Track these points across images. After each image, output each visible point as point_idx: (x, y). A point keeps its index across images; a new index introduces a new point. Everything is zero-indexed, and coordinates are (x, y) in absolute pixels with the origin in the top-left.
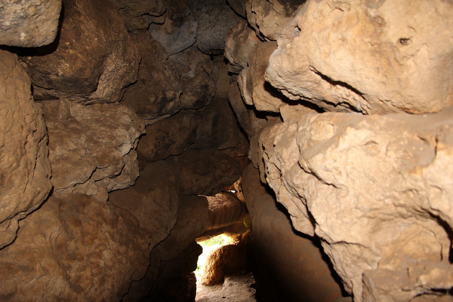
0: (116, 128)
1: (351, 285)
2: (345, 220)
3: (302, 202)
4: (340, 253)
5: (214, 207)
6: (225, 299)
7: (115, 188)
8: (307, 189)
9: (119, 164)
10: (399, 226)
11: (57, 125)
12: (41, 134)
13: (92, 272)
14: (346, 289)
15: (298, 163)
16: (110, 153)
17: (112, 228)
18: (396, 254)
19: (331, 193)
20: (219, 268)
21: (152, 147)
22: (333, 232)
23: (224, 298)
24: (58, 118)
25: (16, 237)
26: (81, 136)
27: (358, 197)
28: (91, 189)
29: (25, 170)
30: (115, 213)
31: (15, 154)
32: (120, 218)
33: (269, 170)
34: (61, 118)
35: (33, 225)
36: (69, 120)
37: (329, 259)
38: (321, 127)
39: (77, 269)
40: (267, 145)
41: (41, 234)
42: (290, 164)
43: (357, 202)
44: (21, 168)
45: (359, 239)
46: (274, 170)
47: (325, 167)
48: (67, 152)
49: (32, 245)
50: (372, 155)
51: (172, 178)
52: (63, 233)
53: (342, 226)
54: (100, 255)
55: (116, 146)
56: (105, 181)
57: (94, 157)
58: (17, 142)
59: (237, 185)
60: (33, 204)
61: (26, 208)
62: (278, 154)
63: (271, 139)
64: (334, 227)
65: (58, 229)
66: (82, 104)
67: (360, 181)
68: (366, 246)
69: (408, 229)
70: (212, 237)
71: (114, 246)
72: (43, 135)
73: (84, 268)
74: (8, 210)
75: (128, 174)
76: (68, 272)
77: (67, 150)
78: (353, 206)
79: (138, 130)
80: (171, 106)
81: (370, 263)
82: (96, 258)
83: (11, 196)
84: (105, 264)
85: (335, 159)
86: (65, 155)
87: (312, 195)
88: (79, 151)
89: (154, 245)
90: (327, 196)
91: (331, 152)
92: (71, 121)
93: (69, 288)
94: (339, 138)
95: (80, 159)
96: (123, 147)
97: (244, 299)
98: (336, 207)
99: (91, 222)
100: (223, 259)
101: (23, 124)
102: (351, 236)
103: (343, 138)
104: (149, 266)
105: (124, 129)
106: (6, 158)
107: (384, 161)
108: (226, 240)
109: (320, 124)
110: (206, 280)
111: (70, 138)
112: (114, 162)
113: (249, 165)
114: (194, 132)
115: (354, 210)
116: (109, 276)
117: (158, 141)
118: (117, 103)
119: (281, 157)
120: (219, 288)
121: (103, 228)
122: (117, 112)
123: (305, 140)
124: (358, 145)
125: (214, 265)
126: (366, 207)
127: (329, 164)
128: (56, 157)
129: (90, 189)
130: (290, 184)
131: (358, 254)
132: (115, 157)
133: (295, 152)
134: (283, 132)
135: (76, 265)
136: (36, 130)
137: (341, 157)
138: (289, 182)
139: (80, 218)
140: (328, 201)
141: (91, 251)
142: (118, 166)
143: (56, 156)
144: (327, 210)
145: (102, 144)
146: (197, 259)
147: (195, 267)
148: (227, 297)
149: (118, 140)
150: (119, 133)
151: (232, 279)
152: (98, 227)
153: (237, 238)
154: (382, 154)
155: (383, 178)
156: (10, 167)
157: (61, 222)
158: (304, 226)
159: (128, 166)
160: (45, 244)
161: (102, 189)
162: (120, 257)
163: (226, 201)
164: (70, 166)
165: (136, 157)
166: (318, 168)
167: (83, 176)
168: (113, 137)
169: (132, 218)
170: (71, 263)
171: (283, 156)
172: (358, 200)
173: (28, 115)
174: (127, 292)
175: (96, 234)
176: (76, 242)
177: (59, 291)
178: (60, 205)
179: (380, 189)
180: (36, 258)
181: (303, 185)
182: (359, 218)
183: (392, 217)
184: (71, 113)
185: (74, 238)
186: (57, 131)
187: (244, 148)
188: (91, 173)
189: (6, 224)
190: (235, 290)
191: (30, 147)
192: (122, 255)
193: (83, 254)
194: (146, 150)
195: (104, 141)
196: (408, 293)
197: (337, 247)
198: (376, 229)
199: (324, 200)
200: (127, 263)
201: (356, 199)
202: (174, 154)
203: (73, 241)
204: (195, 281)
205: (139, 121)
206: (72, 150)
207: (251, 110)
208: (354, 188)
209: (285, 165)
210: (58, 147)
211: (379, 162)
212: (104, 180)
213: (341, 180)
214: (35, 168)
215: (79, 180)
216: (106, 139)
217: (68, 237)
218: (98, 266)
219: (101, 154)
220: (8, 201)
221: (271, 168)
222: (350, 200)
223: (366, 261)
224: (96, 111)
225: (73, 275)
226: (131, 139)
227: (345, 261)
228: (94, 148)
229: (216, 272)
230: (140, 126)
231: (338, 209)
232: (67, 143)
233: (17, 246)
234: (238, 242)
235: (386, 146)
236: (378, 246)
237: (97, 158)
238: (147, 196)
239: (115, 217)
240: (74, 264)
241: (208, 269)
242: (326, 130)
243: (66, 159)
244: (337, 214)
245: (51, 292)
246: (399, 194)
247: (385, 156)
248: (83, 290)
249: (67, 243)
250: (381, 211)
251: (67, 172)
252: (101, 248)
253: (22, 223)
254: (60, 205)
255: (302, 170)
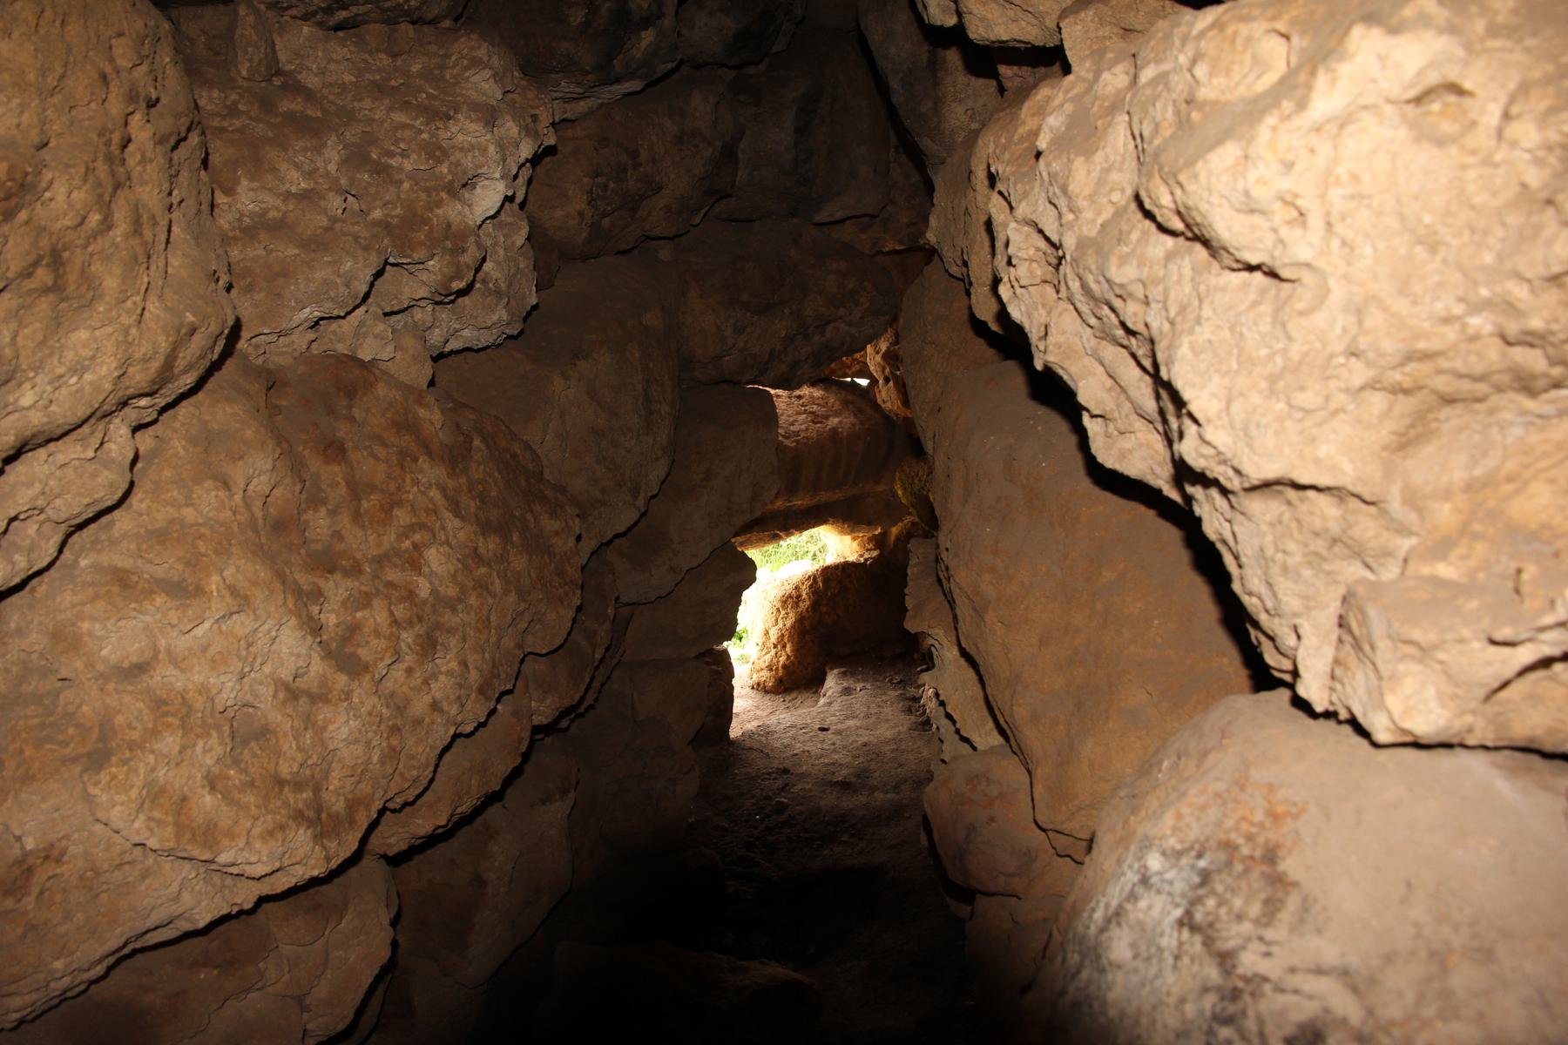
0: (449, 118)
1: (1291, 641)
2: (1301, 398)
3: (1134, 356)
4: (1264, 528)
5: (797, 434)
6: (828, 735)
7: (454, 345)
8: (1160, 298)
9: (464, 250)
10: (1502, 427)
11: (236, 103)
12: (177, 116)
13: (391, 613)
14: (1271, 658)
15: (1138, 199)
16: (431, 210)
17: (453, 474)
18: (1476, 527)
19: (1255, 304)
20: (808, 638)
21: (578, 203)
22: (1250, 445)
23: (822, 729)
24: (233, 73)
25: (132, 484)
26: (324, 145)
27: (1359, 312)
28: (374, 342)
29: (135, 241)
30: (458, 426)
31: (91, 178)
32: (477, 442)
33: (1011, 250)
34: (244, 73)
35: (184, 447)
36: (277, 82)
37: (1218, 556)
38: (1239, 48)
39: (344, 603)
40: (1009, 163)
41: (215, 478)
42: (1099, 213)
43: (1354, 331)
44: (118, 234)
45: (1346, 473)
46: (1032, 252)
47: (1247, 193)
48: (278, 202)
49: (188, 513)
50: (1441, 142)
51: (652, 319)
52: (288, 480)
53: (1288, 424)
54: (414, 562)
55: (451, 183)
56: (418, 315)
57: (375, 223)
58: (94, 136)
59: (878, 358)
60: (176, 371)
61: (153, 382)
62: (1053, 177)
63: (1021, 140)
64: (1258, 425)
65: (269, 466)
66: (320, 24)
67: (1375, 249)
68: (1368, 498)
69: (1533, 438)
70: (789, 534)
71: (462, 535)
72: (185, 121)
73: (365, 601)
74: (92, 383)
75: (498, 293)
76: (315, 609)
77: (278, 195)
78: (1340, 347)
79: (529, 130)
80: (644, 44)
81: (1370, 560)
82: (403, 570)
83: (97, 333)
84: (434, 592)
85: (1291, 157)
86: (273, 214)
87: (1179, 319)
88: (323, 198)
89: (594, 544)
90: (1239, 315)
91: (1274, 129)
92: (284, 86)
93: (322, 658)
94: (1313, 73)
95: (327, 229)
96: (478, 190)
97: (889, 734)
98: (1272, 356)
99: (382, 452)
100: (824, 609)
101: (108, 68)
102: (1317, 461)
103: (1329, 70)
104: (579, 609)
105: (478, 120)
106: (60, 191)
107: (1488, 162)
108: (833, 545)
109: (1236, 33)
110: (765, 674)
111: (286, 150)
112: (448, 244)
113: (927, 270)
114: (729, 154)
115: (1341, 360)
116: (451, 631)
117: (600, 180)
118: (447, 23)
119: (1064, 190)
120: (809, 702)
121: (421, 471)
122: (448, 56)
123: (1165, 108)
124: (1390, 101)
125: (793, 626)
126: (1388, 346)
127: (1264, 180)
128: (240, 220)
129: (370, 340)
130: (1094, 286)
131: (1335, 528)
132: (449, 225)
133: (1120, 170)
134: (1072, 100)
135: (337, 589)
136: (158, 100)
137: (1312, 151)
138: (1090, 279)
139: (340, 434)
140: (1241, 334)
141: (386, 545)
142: (461, 259)
143: (242, 215)
144: (1235, 366)
145: (403, 176)
146: (739, 602)
147: (728, 629)
148: (833, 728)
149: (458, 164)
150: (461, 137)
151: (853, 674)
152: (402, 468)
153: (870, 540)
154: (1482, 138)
155: (1473, 231)
156: (81, 224)
157: (279, 444)
158: (1130, 451)
159: (498, 263)
160: (229, 514)
161: (409, 341)
162: (483, 570)
163: (837, 413)
164: (291, 251)
165: (524, 232)
166: (1215, 199)
167: (342, 289)
168: (441, 148)
169: (517, 448)
170: (321, 583)
171: (1071, 187)
172: (1360, 323)
173: (120, 35)
174: (509, 687)
175: (398, 489)
176: (333, 513)
177: (292, 667)
178: (269, 389)
179: (1455, 277)
180: (206, 555)
181: (1145, 286)
182: (1356, 392)
183: (1482, 388)
184: (282, 57)
185: (324, 502)
186: (237, 123)
187: (905, 220)
188: (369, 278)
189: (92, 434)
190: (859, 708)
191: (144, 161)
192: (489, 566)
193: (359, 556)
194: (559, 213)
195: (408, 166)
196: (1507, 651)
197: (1256, 505)
198: (1412, 432)
199: (1226, 334)
200: (506, 592)
201: (1351, 319)
202: (658, 232)
203: (323, 509)
204: (730, 673)
205: (530, 95)
206: (295, 196)
207: (946, 47)
208: (1346, 277)
209: (1077, 218)
210: (245, 182)
211: (1464, 167)
212: (416, 310)
213: (1302, 247)
214: (168, 242)
215: (329, 305)
216: (414, 156)
217: (303, 496)
218: (410, 595)
219: (398, 211)
220: (88, 353)
221: (1020, 241)
222: (1332, 322)
223: (1357, 552)
224: (370, 53)
225: (331, 620)
226: (504, 161)
227: (1279, 556)
228: (372, 190)
229: (797, 650)
230: (535, 118)
231: (1279, 360)
232: (274, 170)
233: (141, 515)
234: (875, 553)
235: (1503, 99)
236: (1412, 499)
237: (385, 225)
238: (566, 378)
239: (461, 438)
240: (331, 584)
241: (773, 639)
242: (1256, 60)
243: (278, 227)
244: (1273, 379)
245: (267, 669)
246: (1532, 291)
247: (1493, 143)
248: (366, 668)
249: (304, 517)
250: (1443, 363)
251: (285, 274)
252: (417, 537)
253: (145, 440)
254: (269, 389)
255: (1147, 223)
